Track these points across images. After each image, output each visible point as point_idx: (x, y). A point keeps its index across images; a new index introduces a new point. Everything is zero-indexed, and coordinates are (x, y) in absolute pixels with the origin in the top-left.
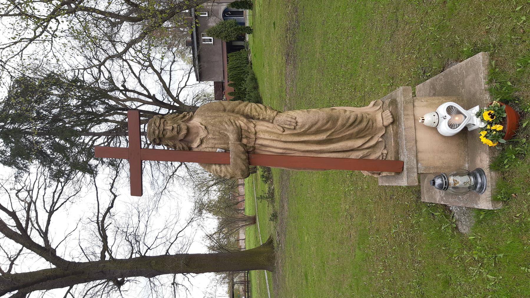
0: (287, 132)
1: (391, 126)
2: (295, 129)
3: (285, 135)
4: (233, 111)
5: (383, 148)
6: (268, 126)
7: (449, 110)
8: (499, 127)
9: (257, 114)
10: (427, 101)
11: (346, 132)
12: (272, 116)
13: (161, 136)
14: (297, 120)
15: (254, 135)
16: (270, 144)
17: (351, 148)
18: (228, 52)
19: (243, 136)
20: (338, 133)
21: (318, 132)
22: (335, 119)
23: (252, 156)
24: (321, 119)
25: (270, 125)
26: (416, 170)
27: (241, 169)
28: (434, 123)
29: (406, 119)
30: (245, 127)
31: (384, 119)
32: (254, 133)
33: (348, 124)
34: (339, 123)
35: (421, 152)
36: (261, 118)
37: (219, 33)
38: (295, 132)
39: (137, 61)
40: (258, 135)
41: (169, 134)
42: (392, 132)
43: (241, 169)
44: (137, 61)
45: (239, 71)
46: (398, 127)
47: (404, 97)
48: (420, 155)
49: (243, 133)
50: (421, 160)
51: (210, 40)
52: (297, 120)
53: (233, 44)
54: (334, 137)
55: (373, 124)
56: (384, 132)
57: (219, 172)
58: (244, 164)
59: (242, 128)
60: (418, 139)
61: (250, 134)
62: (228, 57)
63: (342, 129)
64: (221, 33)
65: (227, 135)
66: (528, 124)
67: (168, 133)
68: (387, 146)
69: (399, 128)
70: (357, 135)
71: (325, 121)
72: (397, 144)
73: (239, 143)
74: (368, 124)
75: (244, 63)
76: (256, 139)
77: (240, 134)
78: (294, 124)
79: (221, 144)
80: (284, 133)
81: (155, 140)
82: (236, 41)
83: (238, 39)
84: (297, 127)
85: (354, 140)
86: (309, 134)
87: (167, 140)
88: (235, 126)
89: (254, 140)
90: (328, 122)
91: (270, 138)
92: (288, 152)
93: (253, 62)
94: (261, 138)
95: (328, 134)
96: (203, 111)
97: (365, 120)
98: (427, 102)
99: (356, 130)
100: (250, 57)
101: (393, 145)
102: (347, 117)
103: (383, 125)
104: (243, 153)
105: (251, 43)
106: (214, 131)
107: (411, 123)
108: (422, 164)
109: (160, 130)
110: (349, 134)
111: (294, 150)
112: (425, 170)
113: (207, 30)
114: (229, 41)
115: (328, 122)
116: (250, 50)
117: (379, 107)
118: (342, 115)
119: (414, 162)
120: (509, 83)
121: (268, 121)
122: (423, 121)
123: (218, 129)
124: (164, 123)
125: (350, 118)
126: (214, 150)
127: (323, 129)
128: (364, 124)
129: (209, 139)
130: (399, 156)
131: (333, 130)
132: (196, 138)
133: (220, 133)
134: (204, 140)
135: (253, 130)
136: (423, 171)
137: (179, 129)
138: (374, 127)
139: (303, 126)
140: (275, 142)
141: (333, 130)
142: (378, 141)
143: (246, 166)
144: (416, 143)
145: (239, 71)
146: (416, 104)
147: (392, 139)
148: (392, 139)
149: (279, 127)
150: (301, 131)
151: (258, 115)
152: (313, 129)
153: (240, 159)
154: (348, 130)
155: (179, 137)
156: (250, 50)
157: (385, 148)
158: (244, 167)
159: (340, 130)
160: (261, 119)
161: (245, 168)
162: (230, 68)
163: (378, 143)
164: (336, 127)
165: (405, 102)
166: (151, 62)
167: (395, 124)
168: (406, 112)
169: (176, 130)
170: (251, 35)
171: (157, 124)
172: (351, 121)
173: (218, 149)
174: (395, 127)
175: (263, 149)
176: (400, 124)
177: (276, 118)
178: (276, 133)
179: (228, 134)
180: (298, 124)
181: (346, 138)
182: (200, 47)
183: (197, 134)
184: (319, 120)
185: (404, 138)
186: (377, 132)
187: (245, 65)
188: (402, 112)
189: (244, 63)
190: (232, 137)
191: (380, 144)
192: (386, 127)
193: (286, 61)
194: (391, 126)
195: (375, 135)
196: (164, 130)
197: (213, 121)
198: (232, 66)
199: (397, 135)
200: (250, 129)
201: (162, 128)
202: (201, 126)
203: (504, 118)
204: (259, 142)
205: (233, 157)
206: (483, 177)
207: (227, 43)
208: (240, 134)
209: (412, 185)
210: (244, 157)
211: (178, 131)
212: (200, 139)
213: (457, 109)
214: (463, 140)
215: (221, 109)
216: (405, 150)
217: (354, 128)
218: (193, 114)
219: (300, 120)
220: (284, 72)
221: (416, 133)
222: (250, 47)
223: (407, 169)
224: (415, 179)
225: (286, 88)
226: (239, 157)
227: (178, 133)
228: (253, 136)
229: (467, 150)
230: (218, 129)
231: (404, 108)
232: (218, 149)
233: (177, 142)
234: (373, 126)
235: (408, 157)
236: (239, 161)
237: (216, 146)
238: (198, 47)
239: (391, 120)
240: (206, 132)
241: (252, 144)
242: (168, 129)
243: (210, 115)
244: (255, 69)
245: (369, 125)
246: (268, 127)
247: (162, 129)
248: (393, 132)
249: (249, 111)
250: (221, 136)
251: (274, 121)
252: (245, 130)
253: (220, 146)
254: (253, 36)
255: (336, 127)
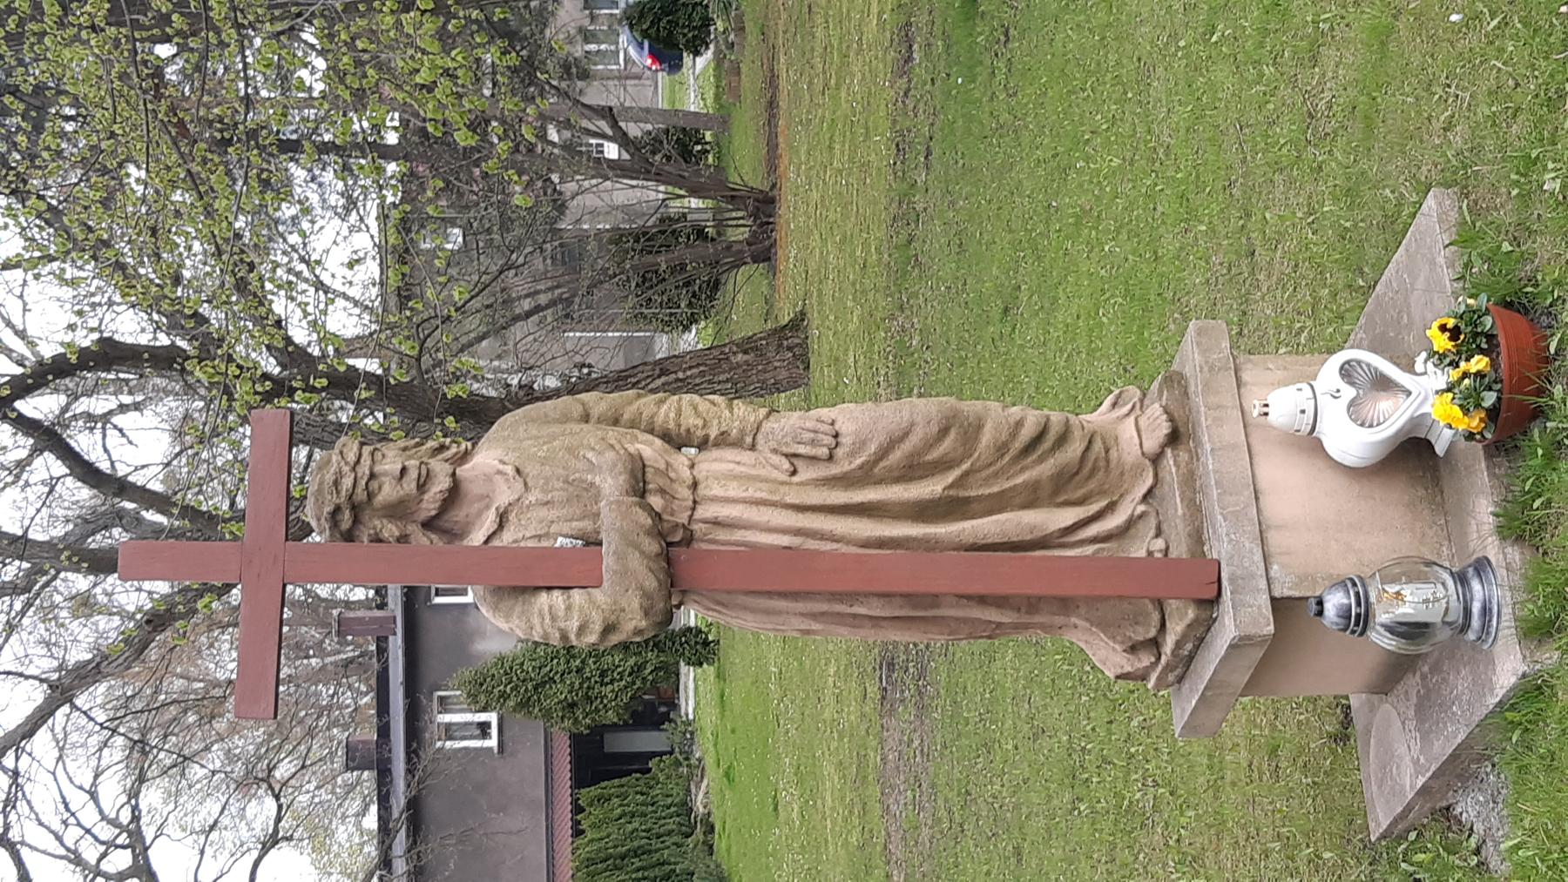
0: (807, 473)
1: (1169, 452)
2: (831, 458)
3: (797, 484)
4: (616, 422)
5: (1152, 533)
6: (738, 459)
7: (1346, 372)
8: (1479, 363)
9: (700, 422)
10: (1285, 368)
11: (1013, 476)
12: (752, 419)
13: (361, 495)
14: (837, 427)
15: (689, 488)
16: (745, 516)
17: (1038, 534)
18: (579, 781)
19: (651, 486)
20: (986, 479)
21: (912, 471)
22: (970, 425)
23: (681, 554)
24: (919, 419)
25: (746, 457)
26: (1263, 584)
27: (642, 588)
28: (1303, 412)
29: (1215, 419)
30: (656, 461)
31: (1143, 433)
32: (690, 482)
33: (1018, 444)
34: (987, 438)
35: (1278, 527)
36: (713, 433)
37: (536, 688)
38: (835, 470)
39: (68, 849)
40: (701, 491)
41: (388, 492)
42: (1174, 470)
43: (642, 588)
44: (68, 849)
45: (640, 874)
46: (1195, 456)
47: (1203, 352)
48: (1274, 538)
49: (649, 476)
50: (1280, 554)
51: (484, 728)
52: (837, 427)
53: (607, 749)
54: (973, 493)
55: (1107, 451)
56: (1149, 482)
57: (561, 614)
58: (650, 570)
59: (647, 463)
60: (1263, 484)
61: (676, 486)
62: (577, 809)
63: (999, 465)
64: (544, 684)
65: (592, 484)
66: (1561, 341)
67: (387, 489)
68: (1165, 527)
69: (1198, 460)
70: (1056, 491)
71: (935, 429)
72: (1195, 510)
73: (635, 499)
74: (1088, 449)
75: (670, 833)
76: (695, 502)
77: (639, 481)
78: (829, 440)
79: (571, 520)
80: (796, 479)
81: (339, 517)
82: (626, 727)
83: (634, 714)
84: (840, 452)
85: (1046, 510)
86: (880, 481)
87: (379, 518)
88: (622, 452)
89: (690, 503)
90: (944, 432)
91: (744, 495)
92: (812, 544)
93: (716, 819)
94: (714, 499)
95: (950, 480)
96: (510, 426)
97: (1077, 433)
98: (1285, 373)
99: (1047, 468)
100: (701, 796)
101: (1180, 512)
102: (1012, 421)
103: (1143, 454)
104: (649, 533)
105: (708, 721)
106: (547, 480)
107: (1233, 431)
108: (1282, 566)
109: (359, 475)
110: (1025, 485)
111: (834, 538)
112: (1296, 586)
113: (467, 674)
114: (588, 727)
115: (944, 432)
116: (700, 760)
117: (1129, 406)
118: (993, 414)
119: (1255, 558)
120: (1506, 247)
121: (737, 444)
122: (1265, 410)
123: (561, 471)
124: (372, 454)
125: (1023, 425)
126: (545, 544)
127: (929, 458)
128: (1074, 450)
129: (528, 507)
130: (1205, 548)
131: (965, 466)
132: (480, 514)
133: (566, 481)
134: (512, 517)
135: (686, 473)
136: (1289, 589)
137: (424, 472)
138: (1113, 465)
139: (861, 445)
140: (762, 508)
141: (965, 466)
142: (1132, 515)
143: (659, 581)
144: (1257, 498)
145: (640, 874)
146: (1246, 376)
147: (1177, 494)
148: (1177, 494)
149: (776, 459)
150: (853, 466)
151: (704, 426)
152: (896, 456)
153: (637, 554)
154: (1022, 470)
155: (424, 505)
156: (700, 760)
157: (1158, 534)
158: (651, 583)
159: (991, 464)
160: (712, 437)
161: (655, 584)
162: (590, 861)
163: (1131, 523)
164: (976, 455)
165: (1206, 369)
166: (146, 849)
167: (1182, 447)
168: (1212, 400)
169: (413, 474)
170: (709, 670)
171: (351, 457)
172: (1027, 433)
173: (560, 539)
174: (1183, 456)
175: (722, 535)
176: (1198, 444)
177: (766, 426)
178: (766, 480)
179: (597, 480)
180: (842, 439)
181: (1018, 501)
182: (426, 756)
183: (487, 499)
184: (912, 424)
185: (1213, 483)
186: (1125, 486)
187: (675, 839)
188: (1200, 400)
189: (670, 833)
190: (611, 484)
191: (1141, 525)
192: (1156, 459)
193: (883, 698)
194: (1169, 452)
195: (1121, 496)
196: (372, 476)
197: (545, 448)
198: (599, 850)
199: (1190, 480)
200: (675, 471)
201: (364, 469)
202: (501, 467)
203: (1490, 337)
204: (704, 512)
205: (613, 547)
206: (1487, 577)
207: (577, 741)
208: (640, 475)
209: (1252, 631)
210: (652, 546)
211: (422, 480)
212: (497, 509)
213: (1368, 365)
214: (1426, 489)
215: (575, 415)
216: (1219, 517)
217: (1041, 460)
218: (474, 446)
219: (845, 427)
220: (874, 758)
221: (1255, 466)
222: (704, 749)
223: (1232, 580)
224: (1261, 614)
225: (888, 834)
226: (637, 547)
227: (422, 486)
228: (684, 493)
229: (1443, 522)
230: (561, 471)
231: (1206, 385)
232: (560, 539)
233: (414, 530)
234: (1108, 461)
235: (1231, 540)
236: (636, 562)
237: (554, 529)
238: (412, 753)
239: (1165, 429)
240: (519, 485)
241: (683, 518)
242: (385, 474)
243: (535, 432)
244: (728, 850)
245: (1092, 456)
246: (738, 463)
247: (367, 472)
248: (1177, 471)
249: (672, 415)
250: (571, 489)
251: (760, 438)
252: (657, 470)
253: (566, 528)
254: (718, 676)
255: (976, 455)
